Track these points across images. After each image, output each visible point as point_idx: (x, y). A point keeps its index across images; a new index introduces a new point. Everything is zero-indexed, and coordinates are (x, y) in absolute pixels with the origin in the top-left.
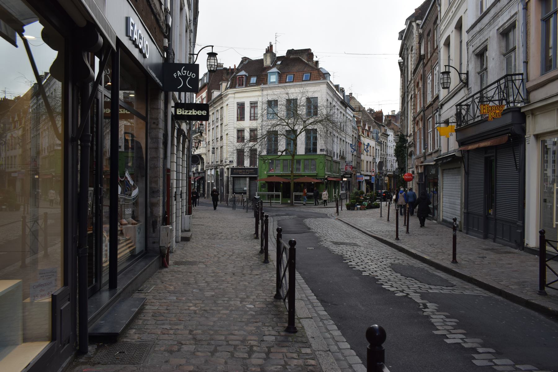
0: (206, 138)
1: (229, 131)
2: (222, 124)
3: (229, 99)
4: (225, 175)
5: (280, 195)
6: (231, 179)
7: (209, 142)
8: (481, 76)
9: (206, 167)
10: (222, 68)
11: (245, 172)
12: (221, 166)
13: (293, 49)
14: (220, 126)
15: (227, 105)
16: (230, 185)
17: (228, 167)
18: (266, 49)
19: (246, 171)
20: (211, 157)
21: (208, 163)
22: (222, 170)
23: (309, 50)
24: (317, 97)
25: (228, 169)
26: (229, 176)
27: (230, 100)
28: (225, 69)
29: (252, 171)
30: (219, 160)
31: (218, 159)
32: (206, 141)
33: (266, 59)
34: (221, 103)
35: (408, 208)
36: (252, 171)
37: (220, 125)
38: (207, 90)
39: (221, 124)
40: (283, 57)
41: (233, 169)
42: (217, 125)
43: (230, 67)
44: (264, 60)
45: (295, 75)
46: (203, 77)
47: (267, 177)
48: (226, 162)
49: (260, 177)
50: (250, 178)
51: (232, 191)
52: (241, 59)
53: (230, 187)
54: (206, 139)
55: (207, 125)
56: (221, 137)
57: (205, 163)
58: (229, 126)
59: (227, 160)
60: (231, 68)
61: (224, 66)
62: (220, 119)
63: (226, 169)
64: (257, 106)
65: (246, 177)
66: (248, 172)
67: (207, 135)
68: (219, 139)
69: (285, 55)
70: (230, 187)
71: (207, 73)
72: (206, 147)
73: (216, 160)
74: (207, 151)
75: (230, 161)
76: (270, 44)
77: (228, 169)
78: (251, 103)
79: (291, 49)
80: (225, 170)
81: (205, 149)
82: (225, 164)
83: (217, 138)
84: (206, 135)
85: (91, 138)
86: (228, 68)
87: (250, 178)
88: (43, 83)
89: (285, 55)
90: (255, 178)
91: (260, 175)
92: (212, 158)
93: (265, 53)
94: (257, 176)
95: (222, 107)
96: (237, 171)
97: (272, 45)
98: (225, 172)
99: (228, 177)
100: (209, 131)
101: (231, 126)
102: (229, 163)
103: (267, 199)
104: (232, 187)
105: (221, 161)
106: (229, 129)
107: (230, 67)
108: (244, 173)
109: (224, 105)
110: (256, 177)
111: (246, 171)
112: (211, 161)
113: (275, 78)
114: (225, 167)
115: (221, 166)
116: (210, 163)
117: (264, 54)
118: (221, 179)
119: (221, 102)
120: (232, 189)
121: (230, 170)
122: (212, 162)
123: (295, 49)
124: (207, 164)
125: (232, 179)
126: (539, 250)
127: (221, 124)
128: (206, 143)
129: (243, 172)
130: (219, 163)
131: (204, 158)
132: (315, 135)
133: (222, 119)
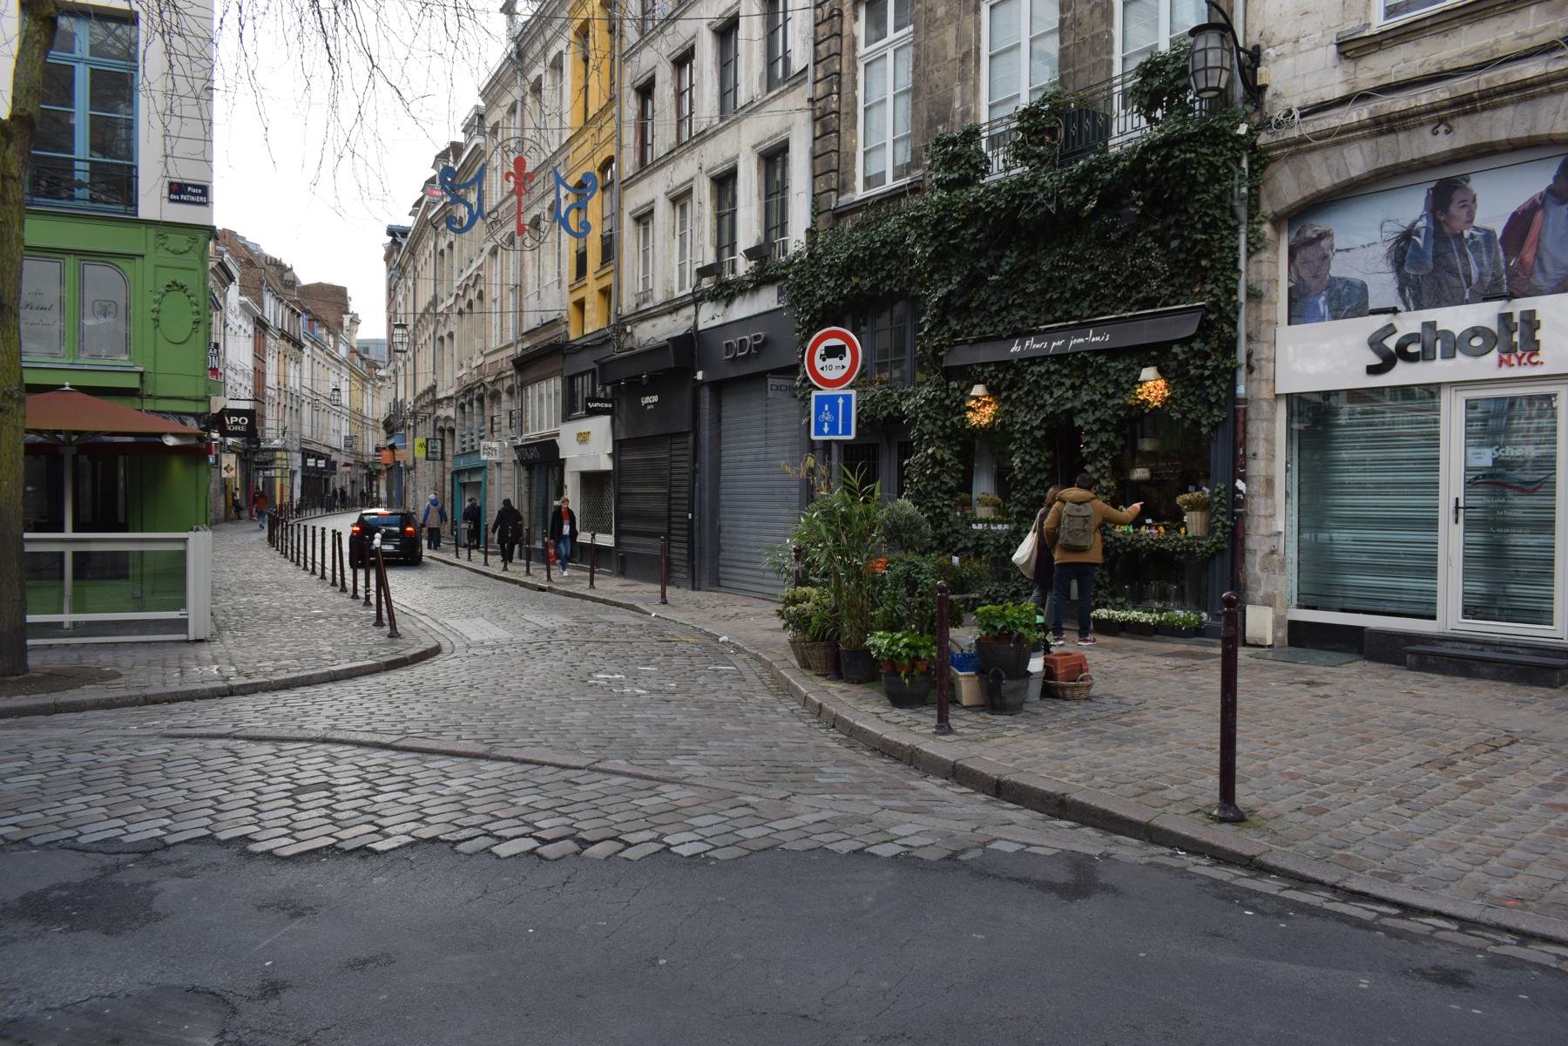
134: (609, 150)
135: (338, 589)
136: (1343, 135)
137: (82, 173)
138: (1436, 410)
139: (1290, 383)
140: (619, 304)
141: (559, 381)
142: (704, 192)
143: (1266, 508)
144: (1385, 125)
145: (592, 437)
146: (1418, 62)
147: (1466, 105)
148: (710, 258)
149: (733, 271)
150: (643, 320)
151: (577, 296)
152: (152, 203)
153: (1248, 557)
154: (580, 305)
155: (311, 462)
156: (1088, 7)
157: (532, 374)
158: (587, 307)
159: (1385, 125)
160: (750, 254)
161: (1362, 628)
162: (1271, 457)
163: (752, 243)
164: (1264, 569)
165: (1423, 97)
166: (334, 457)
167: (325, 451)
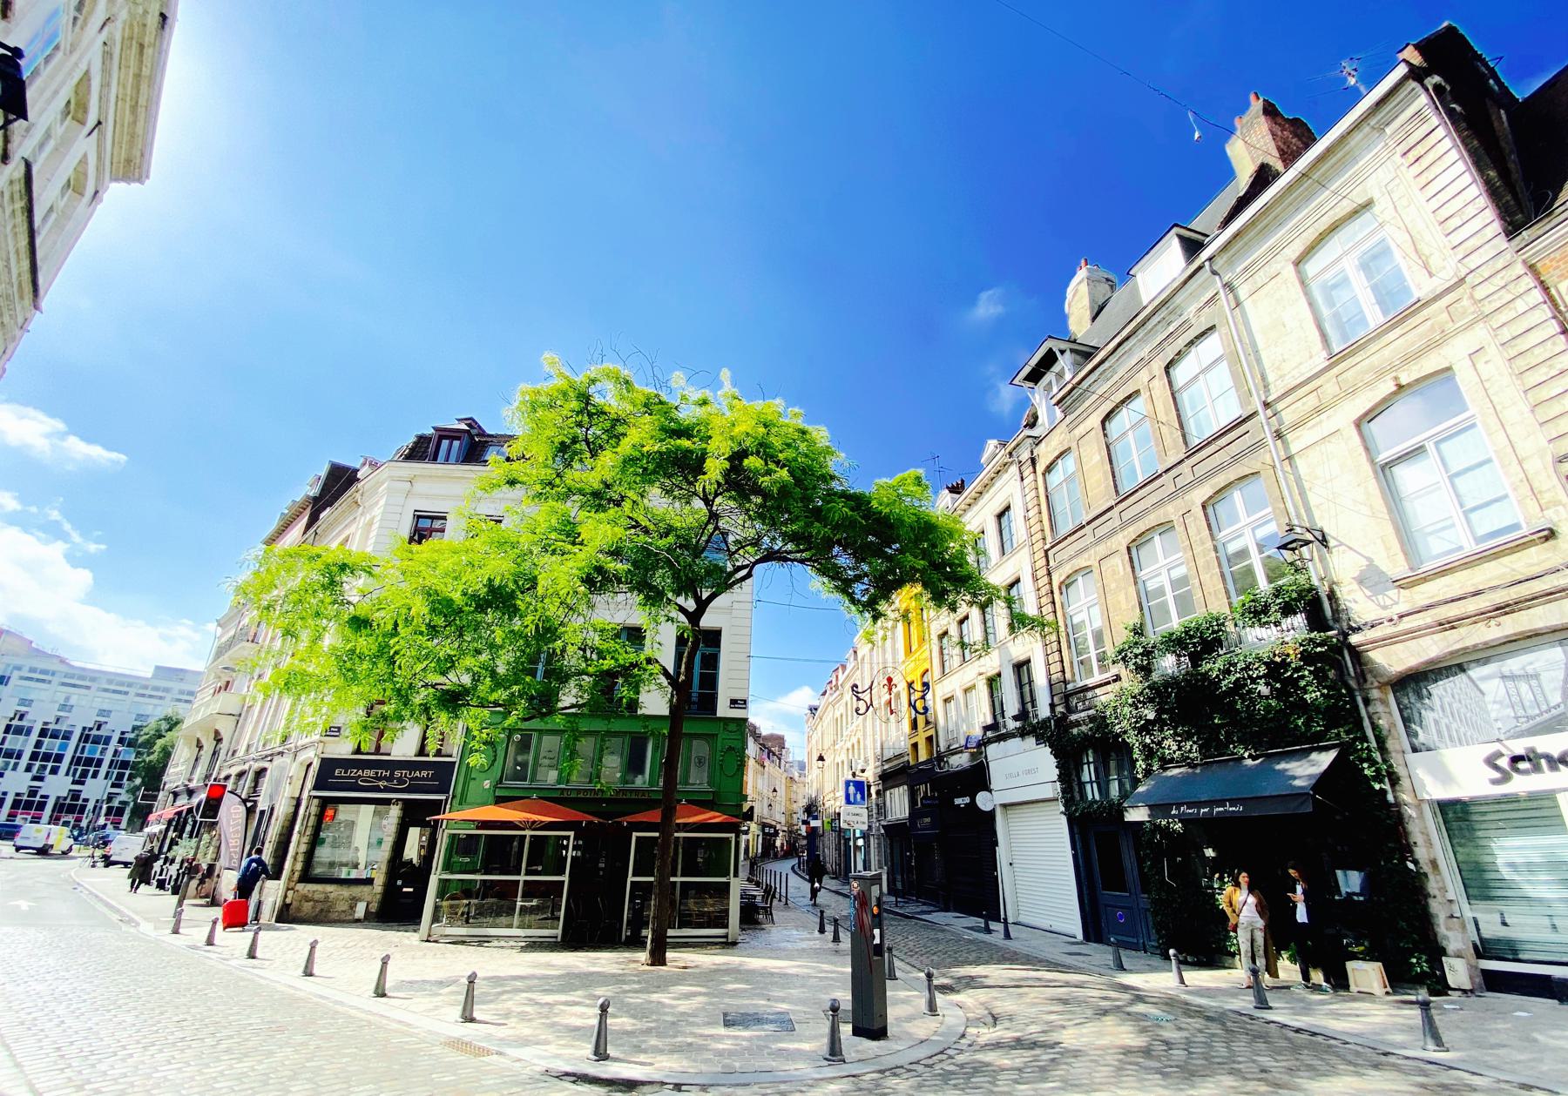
5: (523, 897)
8: (255, 792)
11: (389, 779)
24: (1449, 369)
26: (305, 796)
36: (424, 773)
51: (299, 866)
53: (298, 844)
64: (443, 531)
65: (387, 802)
66: (401, 781)
70: (298, 844)
78: (419, 517)
81: (1320, 360)
85: (1390, 267)
88: (1502, 112)
94: (443, 797)
96: (353, 772)
103: (681, 840)
104: (303, 848)
108: (381, 784)
111: (397, 774)
120: (301, 858)
125: (314, 810)
129: (380, 779)
132: (709, 651)
134: (927, 666)
135: (782, 904)
136: (1412, 634)
137: (695, 697)
138: (1557, 807)
139: (1437, 791)
140: (938, 746)
141: (906, 787)
142: (251, 776)
143: (1437, 882)
144: (1449, 625)
145: (816, 758)
146: (1458, 586)
147: (1503, 609)
148: (989, 721)
149: (1005, 727)
150: (953, 754)
151: (913, 741)
152: (723, 710)
153: (1436, 921)
154: (915, 746)
155: (767, 830)
156: (1209, 576)
157: (890, 783)
158: (919, 747)
159: (1449, 625)
160: (1015, 718)
161: (1549, 976)
162: (1430, 844)
163: (1016, 713)
164: (1448, 929)
165: (1472, 606)
166: (778, 827)
167: (774, 823)
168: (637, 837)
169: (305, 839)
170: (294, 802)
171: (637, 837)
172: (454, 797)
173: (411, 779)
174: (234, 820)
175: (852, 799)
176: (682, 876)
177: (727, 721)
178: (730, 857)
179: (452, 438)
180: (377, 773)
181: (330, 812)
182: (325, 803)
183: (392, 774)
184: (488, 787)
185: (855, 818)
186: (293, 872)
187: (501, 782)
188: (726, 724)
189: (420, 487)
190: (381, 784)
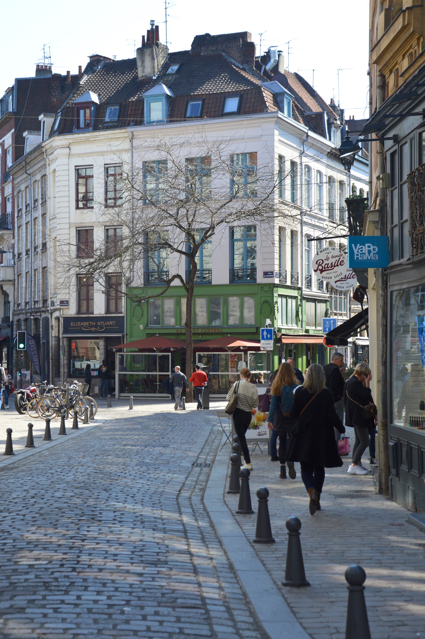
0: (13, 245)
1: (59, 232)
2: (45, 213)
3: (56, 159)
4: (53, 333)
6: (64, 343)
7: (20, 254)
9: (13, 315)
10: (49, 76)
11: (96, 326)
12: (43, 311)
13: (208, 35)
14: (40, 219)
15: (54, 171)
16: (62, 357)
17: (56, 314)
18: (143, 37)
19: (99, 323)
20: (24, 289)
21: (19, 305)
22: (47, 320)
23: (244, 35)
25: (58, 319)
26: (61, 336)
27: (58, 162)
28: (58, 77)
29: (111, 323)
30: (41, 298)
31: (39, 297)
32: (13, 253)
33: (143, 62)
34: (42, 166)
35: (176, 408)
36: (111, 323)
37: (40, 216)
38: (13, 130)
39: (44, 215)
40: (186, 52)
41: (68, 320)
42: (35, 215)
43: (68, 72)
44: (139, 63)
45: (206, 101)
46: (5, 96)
47: (145, 337)
48: (53, 303)
49: (128, 337)
50: (107, 339)
52: (88, 60)
54: (13, 248)
55: (16, 215)
56: (44, 245)
57: (12, 304)
58: (58, 221)
59: (55, 300)
60: (72, 73)
61: (54, 71)
62: (40, 201)
63: (53, 320)
66: (101, 327)
67: (16, 238)
68: (39, 250)
69: (189, 48)
71: (13, 87)
72: (14, 267)
73: (34, 298)
74: (16, 276)
75: (62, 302)
76: (152, 25)
77: (58, 319)
79: (203, 33)
80: (54, 322)
81: (12, 269)
82: (52, 308)
83: (36, 248)
84: (14, 238)
86: (64, 73)
87: (107, 339)
89: (189, 48)
90: (119, 340)
91: (128, 333)
92: (26, 294)
93: (140, 46)
95: (45, 175)
97: (157, 27)
98: (52, 326)
99: (58, 338)
100: (19, 227)
101: (62, 221)
102: (58, 307)
105: (45, 301)
106: (58, 227)
107: (68, 72)
108: (93, 329)
109: (49, 170)
110: (119, 337)
111: (99, 323)
112: (23, 301)
113: (161, 108)
114: (51, 314)
115: (43, 311)
116: (23, 306)
117: (138, 50)
118: (44, 343)
119: (42, 163)
120: (66, 367)
121: (62, 320)
122: (26, 303)
123: (212, 34)
124: (16, 306)
125: (65, 343)
126: (341, 457)
127: (44, 215)
128: (14, 256)
129: (92, 326)
130: (41, 305)
131: (8, 292)
133: (44, 203)
152: (260, 279)
168: (169, 355)
169: (65, 358)
170: (57, 339)
171: (169, 355)
172: (127, 335)
173: (105, 326)
174: (32, 348)
175: (265, 337)
176: (160, 371)
177: (263, 285)
178: (139, 355)
179: (84, 108)
180: (89, 324)
181: (73, 345)
182: (70, 339)
183: (96, 324)
184: (142, 328)
185: (267, 346)
186: (64, 373)
187: (148, 326)
188: (262, 288)
189: (75, 149)
190: (93, 329)
